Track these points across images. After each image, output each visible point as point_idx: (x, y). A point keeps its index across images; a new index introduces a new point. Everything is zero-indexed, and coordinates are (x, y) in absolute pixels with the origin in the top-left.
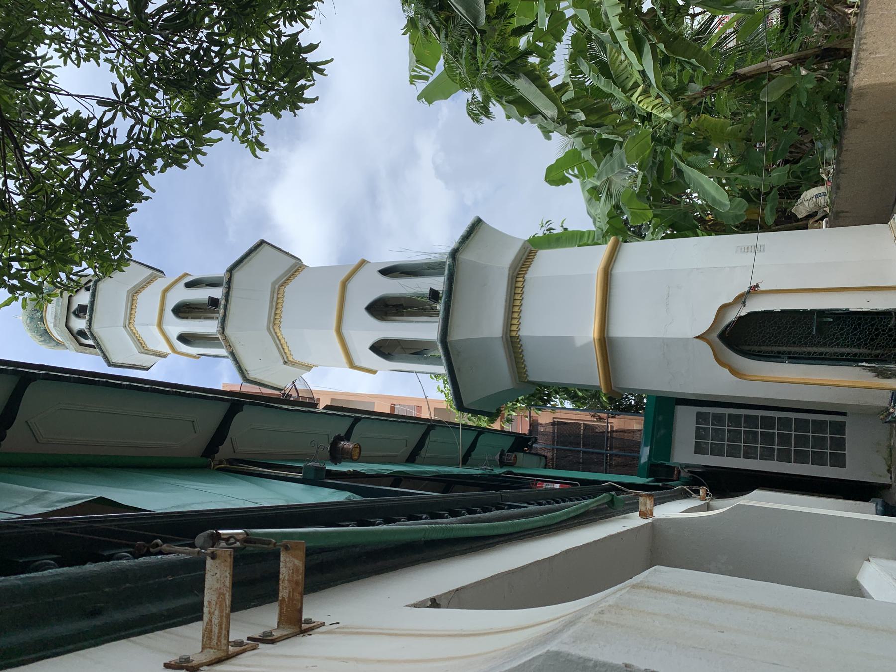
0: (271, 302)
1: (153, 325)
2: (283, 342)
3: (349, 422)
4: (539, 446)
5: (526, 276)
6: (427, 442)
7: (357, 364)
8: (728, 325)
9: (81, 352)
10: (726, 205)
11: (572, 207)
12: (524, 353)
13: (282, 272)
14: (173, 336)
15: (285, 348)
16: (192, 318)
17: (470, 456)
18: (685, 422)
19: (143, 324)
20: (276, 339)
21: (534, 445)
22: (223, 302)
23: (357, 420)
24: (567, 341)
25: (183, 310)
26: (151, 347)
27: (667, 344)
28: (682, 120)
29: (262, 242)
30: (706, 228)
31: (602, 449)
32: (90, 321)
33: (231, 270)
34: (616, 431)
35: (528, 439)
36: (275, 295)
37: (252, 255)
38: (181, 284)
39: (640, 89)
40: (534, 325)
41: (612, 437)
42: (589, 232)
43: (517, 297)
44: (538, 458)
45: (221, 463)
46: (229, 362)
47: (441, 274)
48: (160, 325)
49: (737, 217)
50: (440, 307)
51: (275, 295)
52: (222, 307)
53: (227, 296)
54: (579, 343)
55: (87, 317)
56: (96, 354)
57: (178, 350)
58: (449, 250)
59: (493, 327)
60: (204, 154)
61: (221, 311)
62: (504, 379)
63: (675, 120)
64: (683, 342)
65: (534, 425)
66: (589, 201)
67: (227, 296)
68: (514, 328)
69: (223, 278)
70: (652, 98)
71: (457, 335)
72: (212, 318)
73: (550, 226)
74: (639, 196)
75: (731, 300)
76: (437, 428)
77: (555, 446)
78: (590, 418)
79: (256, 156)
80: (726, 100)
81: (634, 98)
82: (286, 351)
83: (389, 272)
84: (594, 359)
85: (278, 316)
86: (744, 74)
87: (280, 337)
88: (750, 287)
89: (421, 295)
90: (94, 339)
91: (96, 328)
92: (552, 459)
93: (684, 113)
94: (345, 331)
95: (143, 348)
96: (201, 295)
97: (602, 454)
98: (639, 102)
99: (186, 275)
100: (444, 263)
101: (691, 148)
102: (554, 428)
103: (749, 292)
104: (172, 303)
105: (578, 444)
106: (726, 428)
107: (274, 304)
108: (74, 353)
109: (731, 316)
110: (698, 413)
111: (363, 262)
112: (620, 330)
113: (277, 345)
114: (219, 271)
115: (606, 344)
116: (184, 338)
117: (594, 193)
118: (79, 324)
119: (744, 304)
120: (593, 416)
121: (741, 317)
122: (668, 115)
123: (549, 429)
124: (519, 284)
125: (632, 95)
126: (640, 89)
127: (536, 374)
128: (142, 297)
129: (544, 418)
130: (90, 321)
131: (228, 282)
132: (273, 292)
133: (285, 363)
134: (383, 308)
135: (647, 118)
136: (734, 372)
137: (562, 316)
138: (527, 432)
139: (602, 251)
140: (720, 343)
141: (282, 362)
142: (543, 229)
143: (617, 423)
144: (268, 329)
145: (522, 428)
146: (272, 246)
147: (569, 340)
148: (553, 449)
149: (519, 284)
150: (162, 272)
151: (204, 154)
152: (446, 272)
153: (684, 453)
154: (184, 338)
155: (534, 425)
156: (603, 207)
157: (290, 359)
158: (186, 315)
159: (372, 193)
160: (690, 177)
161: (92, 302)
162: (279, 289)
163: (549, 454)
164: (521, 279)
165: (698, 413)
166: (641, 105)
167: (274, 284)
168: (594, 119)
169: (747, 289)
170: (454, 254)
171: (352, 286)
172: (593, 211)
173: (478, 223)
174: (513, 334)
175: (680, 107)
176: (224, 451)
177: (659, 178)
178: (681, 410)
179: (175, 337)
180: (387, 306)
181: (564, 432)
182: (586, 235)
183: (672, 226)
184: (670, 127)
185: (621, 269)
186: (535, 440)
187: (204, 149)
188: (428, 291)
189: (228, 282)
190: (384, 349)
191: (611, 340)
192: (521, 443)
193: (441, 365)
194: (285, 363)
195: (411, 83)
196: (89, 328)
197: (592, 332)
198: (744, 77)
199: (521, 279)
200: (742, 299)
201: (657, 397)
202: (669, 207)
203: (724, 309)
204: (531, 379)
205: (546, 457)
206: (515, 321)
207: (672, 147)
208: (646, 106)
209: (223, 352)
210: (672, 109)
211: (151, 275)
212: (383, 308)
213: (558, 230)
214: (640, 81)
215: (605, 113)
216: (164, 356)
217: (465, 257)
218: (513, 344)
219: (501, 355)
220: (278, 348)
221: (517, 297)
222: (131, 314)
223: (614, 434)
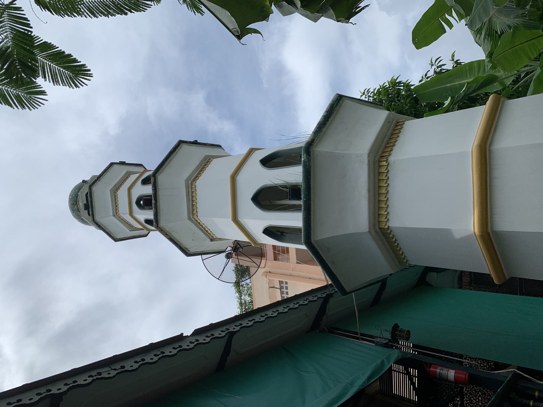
0: (188, 195)
2: (204, 226)
5: (391, 159)
14: (143, 221)
25: (266, 199)
36: (190, 190)
37: (172, 156)
51: (190, 190)
54: (458, 235)
59: (359, 220)
71: (321, 234)
73: (440, 64)
112: (508, 221)
132: (187, 187)
141: (209, 240)
142: (434, 67)
144: (189, 219)
147: (446, 233)
150: (219, 146)
171: (240, 178)
174: (383, 225)
185: (506, 141)
191: (498, 234)
194: (212, 240)
197: (469, 224)
199: (384, 163)
218: (383, 234)
220: (202, 231)
222: (193, 205)
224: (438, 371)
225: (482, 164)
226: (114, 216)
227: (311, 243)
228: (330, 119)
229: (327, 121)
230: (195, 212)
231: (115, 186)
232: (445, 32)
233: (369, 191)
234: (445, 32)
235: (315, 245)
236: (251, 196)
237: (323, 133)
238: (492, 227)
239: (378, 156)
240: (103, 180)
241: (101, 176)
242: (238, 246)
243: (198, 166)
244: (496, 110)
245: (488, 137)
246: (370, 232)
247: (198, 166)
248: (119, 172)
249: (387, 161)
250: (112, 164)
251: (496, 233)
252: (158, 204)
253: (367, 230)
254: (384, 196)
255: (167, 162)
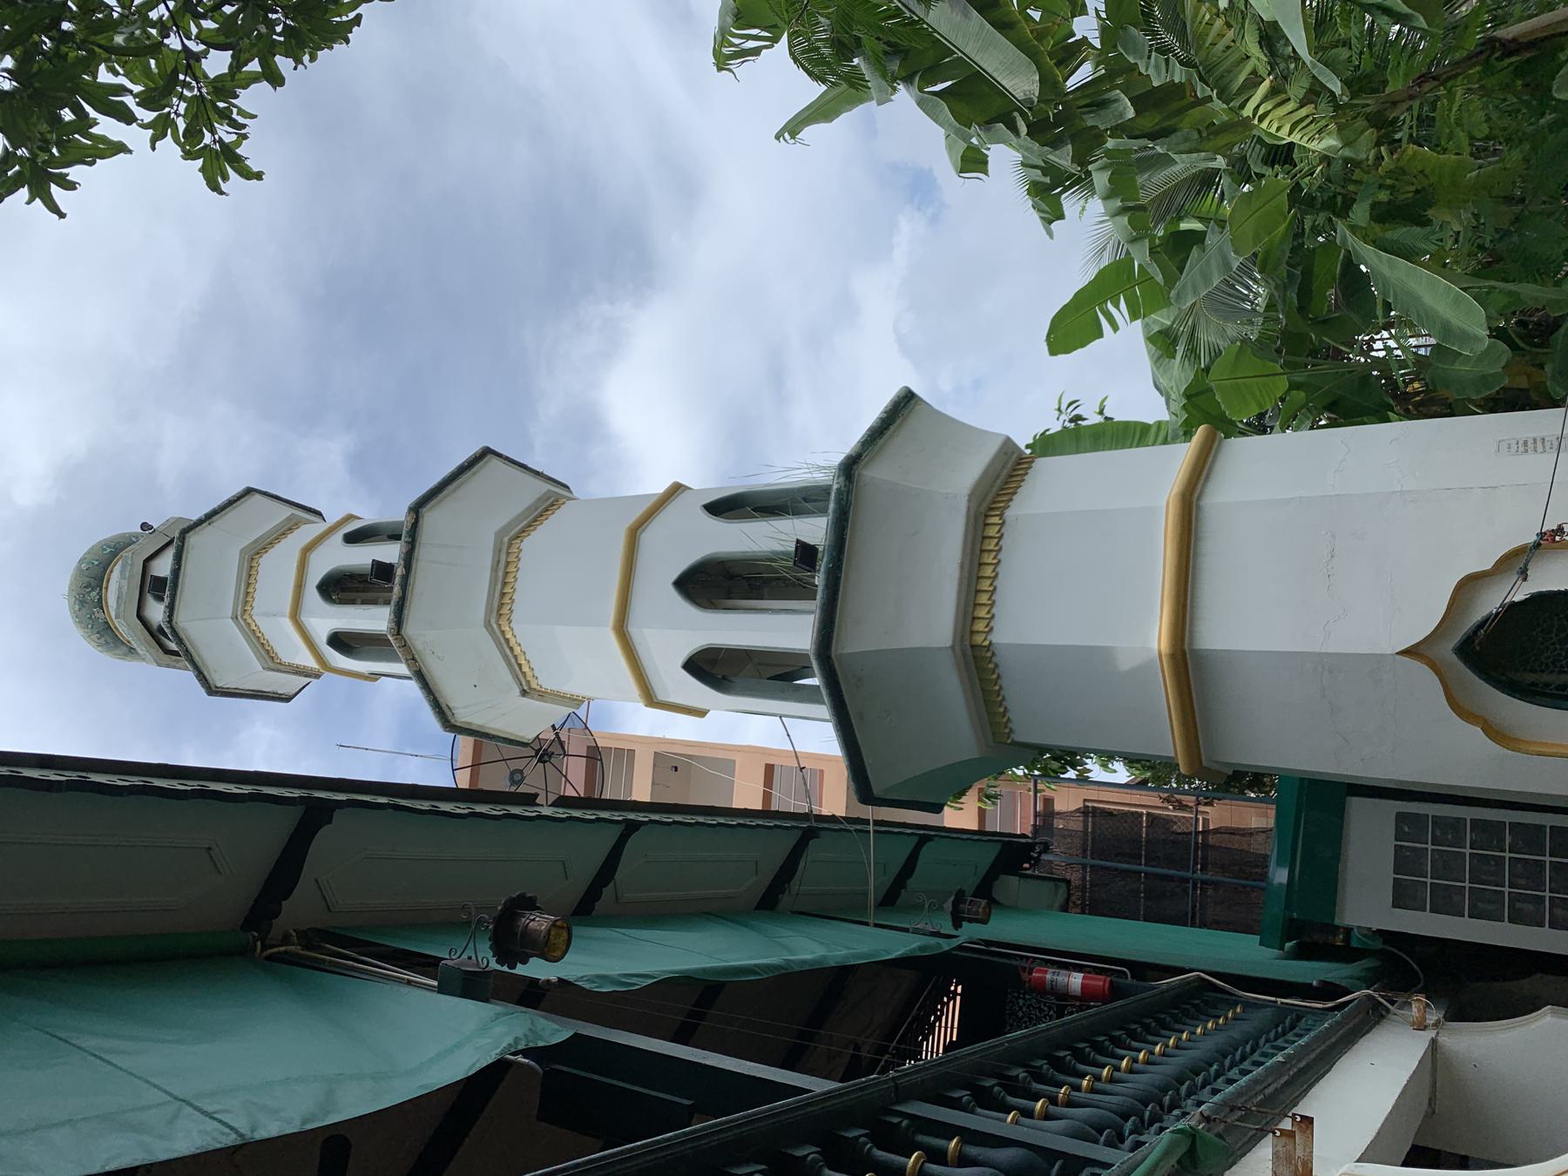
0: (495, 569)
1: (283, 615)
2: (517, 650)
3: (613, 834)
4: (1056, 858)
5: (1008, 513)
6: (802, 864)
7: (661, 697)
8: (1481, 625)
9: (168, 666)
10: (1477, 339)
11: (1123, 373)
12: (1004, 682)
13: (520, 509)
14: (321, 638)
15: (523, 662)
16: (364, 602)
17: (904, 886)
18: (1370, 840)
19: (267, 614)
20: (506, 647)
21: (1044, 857)
22: (399, 571)
23: (632, 827)
24: (1095, 659)
26: (286, 657)
27: (1331, 669)
28: (1365, 150)
29: (486, 452)
30: (1407, 410)
31: (1186, 868)
32: (171, 609)
33: (417, 508)
34: (1217, 831)
35: (1031, 847)
36: (503, 557)
37: (464, 477)
38: (338, 537)
39: (1265, 86)
40: (1027, 620)
41: (1205, 845)
42: (1159, 423)
43: (988, 558)
44: (1051, 884)
45: (286, 940)
46: (413, 687)
47: (824, 511)
48: (295, 616)
49: (1484, 380)
50: (819, 580)
51: (503, 557)
52: (397, 580)
53: (408, 558)
54: (1125, 663)
55: (167, 600)
56: (186, 669)
57: (334, 664)
58: (838, 458)
59: (932, 623)
60: (71, 186)
61: (397, 589)
62: (960, 737)
63: (1347, 153)
64: (1377, 660)
65: (1047, 815)
66: (1157, 361)
67: (408, 558)
68: (980, 626)
69: (402, 523)
70: (1290, 106)
71: (854, 641)
72: (374, 602)
74: (1261, 347)
75: (1488, 565)
76: (822, 833)
77: (1089, 861)
78: (1158, 803)
79: (222, 193)
80: (1466, 109)
81: (1247, 111)
82: (525, 669)
83: (724, 508)
84: (1161, 694)
85: (506, 600)
86: (1514, 40)
87: (512, 642)
88: (1542, 535)
89: (774, 557)
90: (180, 642)
91: (183, 620)
92: (1083, 888)
93: (1370, 134)
94: (634, 630)
95: (271, 661)
96: (362, 557)
97: (1186, 880)
98: (1261, 119)
99: (350, 518)
100: (830, 487)
101: (1385, 214)
102: (1085, 823)
103: (1537, 545)
104: (316, 574)
105: (1136, 858)
106: (1468, 851)
107: (500, 574)
108: (154, 668)
109: (1490, 602)
110: (1398, 814)
111: (677, 489)
112: (1219, 633)
113: (505, 657)
114: (397, 513)
115: (1187, 663)
116: (340, 641)
117: (1163, 343)
118: (156, 612)
119: (1524, 575)
120: (1167, 800)
121: (1513, 605)
122: (1330, 142)
123: (1076, 825)
124: (992, 531)
125: (1242, 106)
126: (1265, 86)
127: (1026, 732)
128: (267, 562)
129: (1067, 800)
130: (171, 609)
131: (409, 534)
132: (498, 550)
133: (524, 693)
134: (709, 584)
135: (1281, 155)
136: (1495, 733)
137: (1088, 596)
138: (1028, 831)
139: (1182, 454)
140: (1461, 665)
141: (517, 691)
143: (1218, 815)
144: (488, 625)
145: (1021, 823)
146: (507, 459)
148: (1084, 867)
149: (992, 531)
150: (318, 514)
151: (71, 186)
152: (832, 506)
153: (1367, 904)
154: (340, 641)
155: (1047, 815)
156: (1180, 373)
157: (534, 685)
158: (353, 595)
159: (777, 375)
160: (1385, 285)
161: (176, 572)
162: (510, 545)
163: (1075, 877)
164: (996, 520)
165: (1398, 814)
166: (1264, 125)
167: (499, 535)
168: (1150, 121)
169: (1533, 538)
170: (850, 467)
171: (648, 537)
172: (1163, 382)
173: (906, 402)
174: (979, 639)
175: (1361, 123)
176: (298, 909)
177: (1302, 309)
178: (1355, 804)
179: (325, 639)
180: (731, 577)
181: (1107, 831)
182: (1153, 430)
183: (1330, 407)
184: (1337, 167)
185: (1221, 496)
186: (1046, 848)
187: (74, 173)
188: (791, 548)
189: (409, 534)
190: (713, 668)
191: (1201, 658)
192: (1014, 855)
193: (820, 702)
194: (524, 693)
195: (720, 69)
196: (170, 622)
197: (1156, 637)
198: (1511, 47)
199: (996, 520)
200: (1517, 561)
201: (1302, 780)
202: (1327, 367)
203: (1469, 586)
204: (1020, 737)
205: (1068, 882)
206: (982, 613)
207: (1344, 211)
208: (1278, 126)
209: (401, 668)
210: (1340, 129)
211: (289, 519)
212: (709, 584)
213: (1093, 419)
214: (1263, 70)
215: (1176, 105)
216: (317, 676)
217: (875, 473)
218: (977, 660)
219: (951, 687)
221: (988, 558)
223: (1211, 840)
224: (1049, 976)
225: (1183, 526)
226: (235, 618)
227: (829, 657)
228: (892, 428)
229: (886, 429)
230: (505, 610)
231: (256, 541)
232: (1101, 335)
233: (962, 567)
234: (1101, 335)
235: (836, 665)
236: (675, 576)
237: (876, 448)
238: (1191, 644)
239: (985, 506)
240: (220, 522)
241: (200, 522)
242: (557, 750)
243: (534, 507)
244: (1210, 448)
245: (1205, 461)
246: (953, 647)
247: (528, 509)
248: (259, 519)
249: (1001, 516)
250: (249, 491)
251: (1193, 651)
252: (411, 580)
253: (949, 644)
254: (988, 582)
255: (450, 488)
